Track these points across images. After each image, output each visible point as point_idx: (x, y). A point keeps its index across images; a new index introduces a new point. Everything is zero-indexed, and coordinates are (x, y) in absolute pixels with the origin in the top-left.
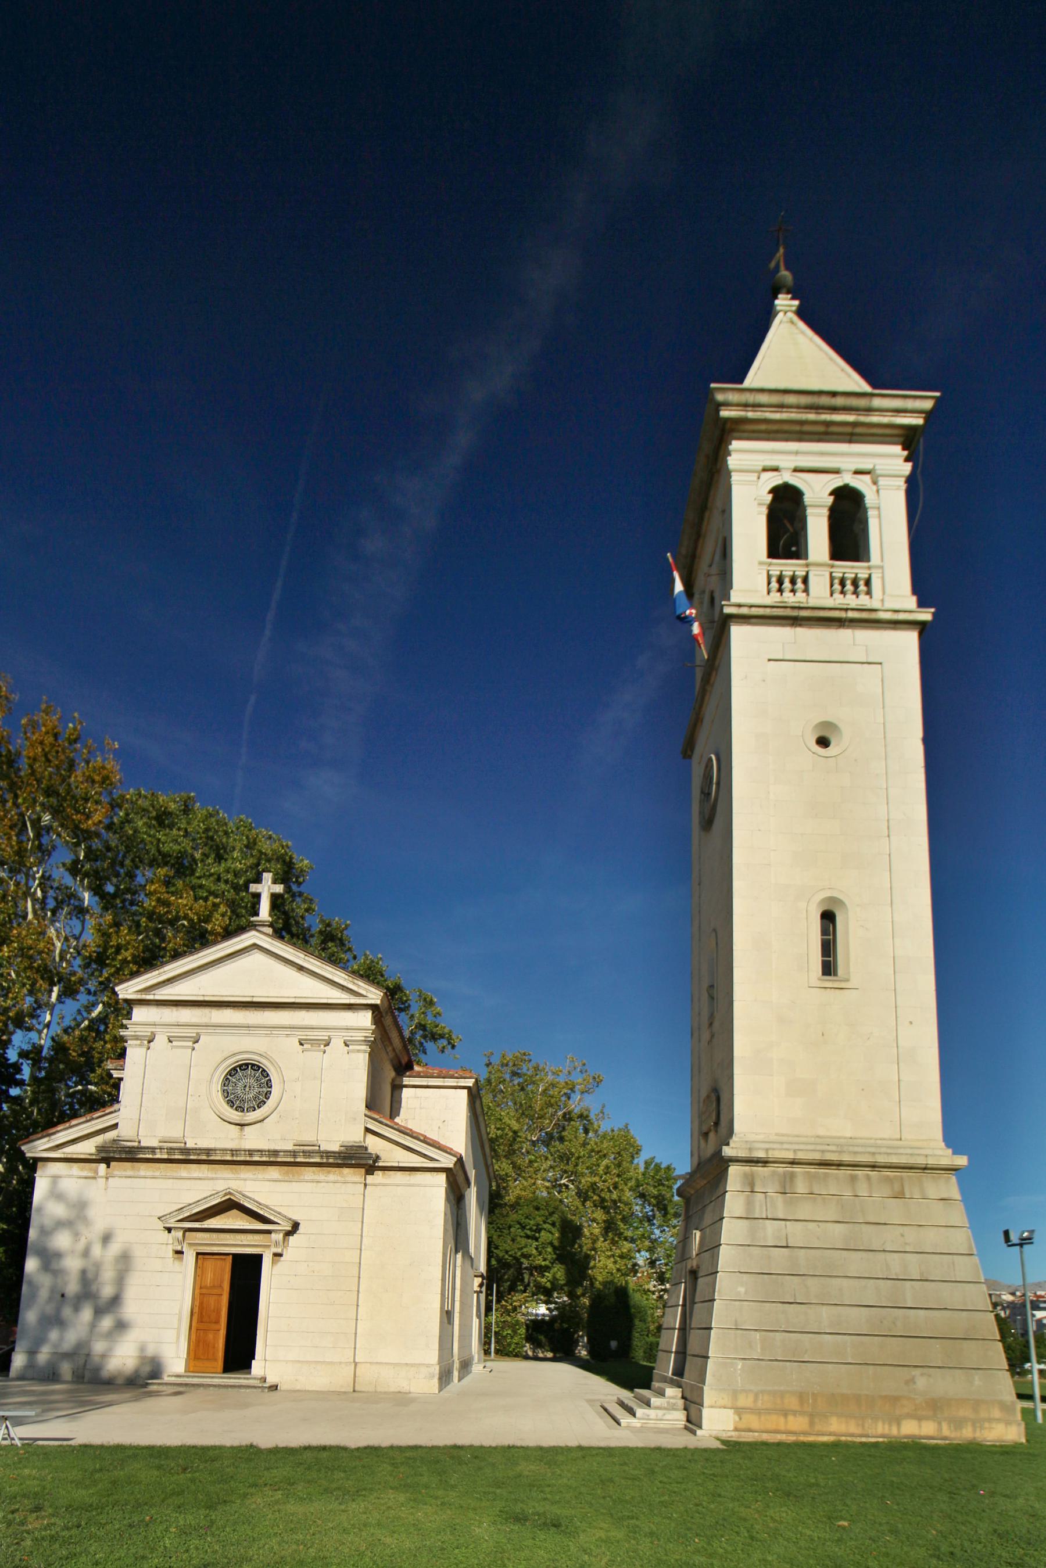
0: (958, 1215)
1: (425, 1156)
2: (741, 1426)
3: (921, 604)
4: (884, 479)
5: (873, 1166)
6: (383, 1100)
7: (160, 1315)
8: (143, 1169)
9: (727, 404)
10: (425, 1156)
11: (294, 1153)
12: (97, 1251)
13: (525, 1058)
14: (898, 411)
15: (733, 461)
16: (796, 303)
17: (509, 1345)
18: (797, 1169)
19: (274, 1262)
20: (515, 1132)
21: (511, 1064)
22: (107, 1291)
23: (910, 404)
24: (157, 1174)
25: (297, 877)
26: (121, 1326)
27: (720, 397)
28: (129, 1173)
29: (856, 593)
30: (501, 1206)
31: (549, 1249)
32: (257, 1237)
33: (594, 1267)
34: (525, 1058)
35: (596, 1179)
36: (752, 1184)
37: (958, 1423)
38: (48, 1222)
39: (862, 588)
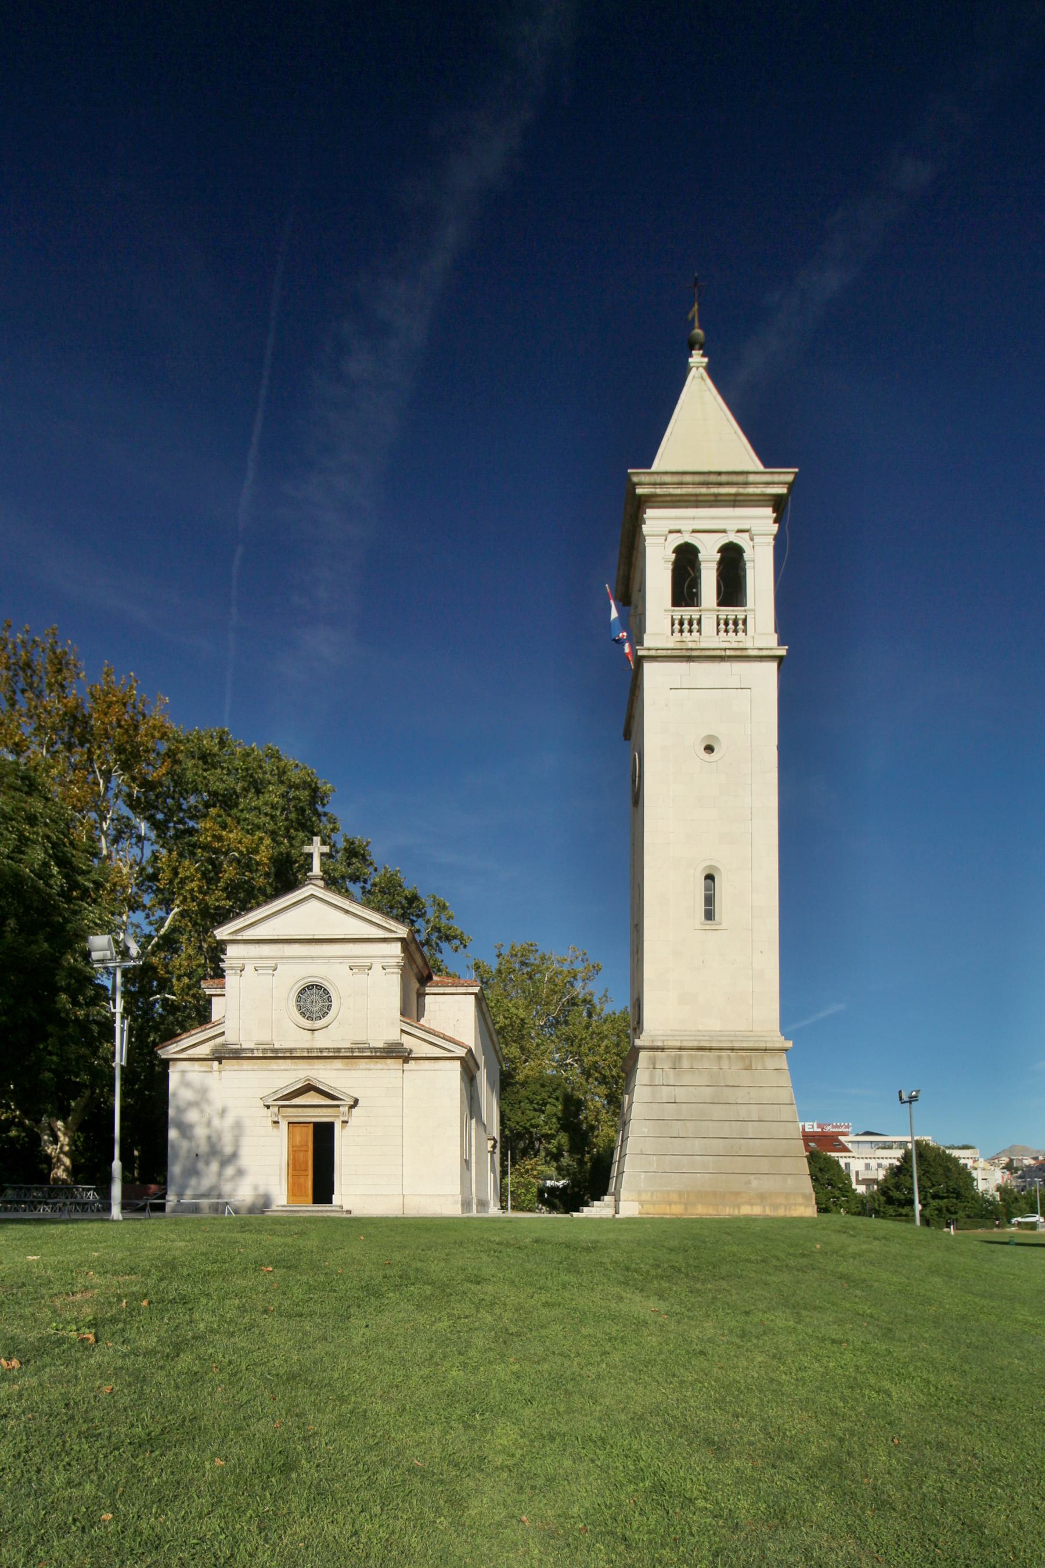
0: (785, 1079)
1: (444, 1049)
2: (643, 1211)
3: (781, 642)
4: (757, 533)
5: (732, 1049)
6: (412, 1007)
7: (263, 1170)
9: (640, 484)
10: (444, 1049)
11: (352, 1050)
12: (216, 1122)
13: (532, 949)
14: (768, 483)
15: (646, 529)
16: (706, 360)
17: (523, 1202)
18: (684, 1053)
19: (342, 1127)
20: (522, 1020)
21: (519, 954)
22: (228, 1150)
23: (776, 478)
24: (256, 1067)
25: (322, 799)
26: (240, 1173)
27: (635, 479)
28: (236, 1067)
29: (736, 631)
30: (513, 1084)
31: (554, 1120)
32: (329, 1110)
33: (597, 1137)
34: (532, 949)
35: (597, 1058)
36: (654, 1064)
37: (775, 1207)
38: (182, 1104)
39: (741, 626)
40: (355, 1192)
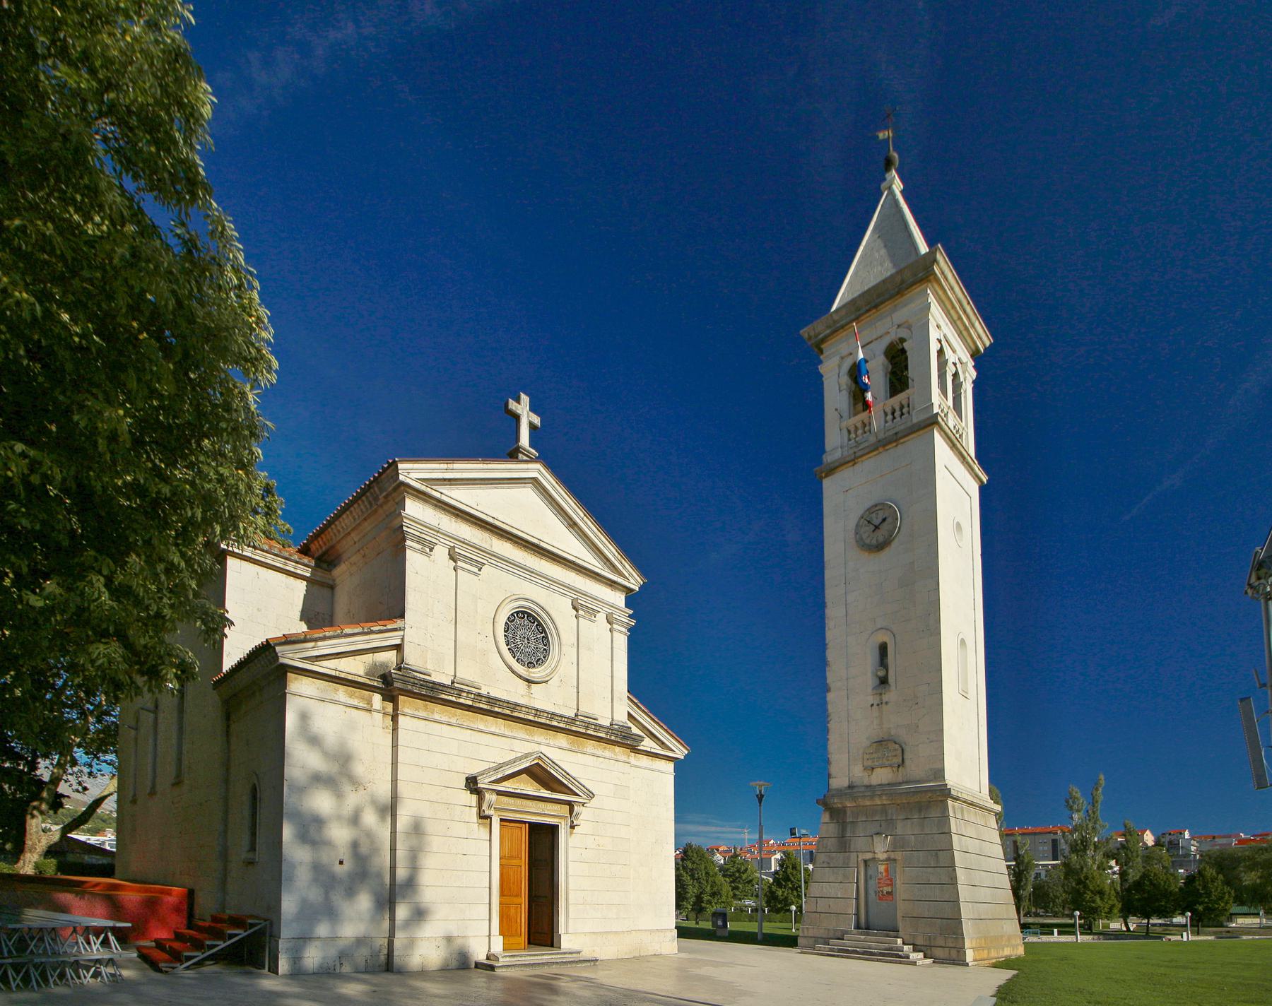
8: (439, 712)
26: (420, 914)
28: (423, 714)
40: (578, 929)
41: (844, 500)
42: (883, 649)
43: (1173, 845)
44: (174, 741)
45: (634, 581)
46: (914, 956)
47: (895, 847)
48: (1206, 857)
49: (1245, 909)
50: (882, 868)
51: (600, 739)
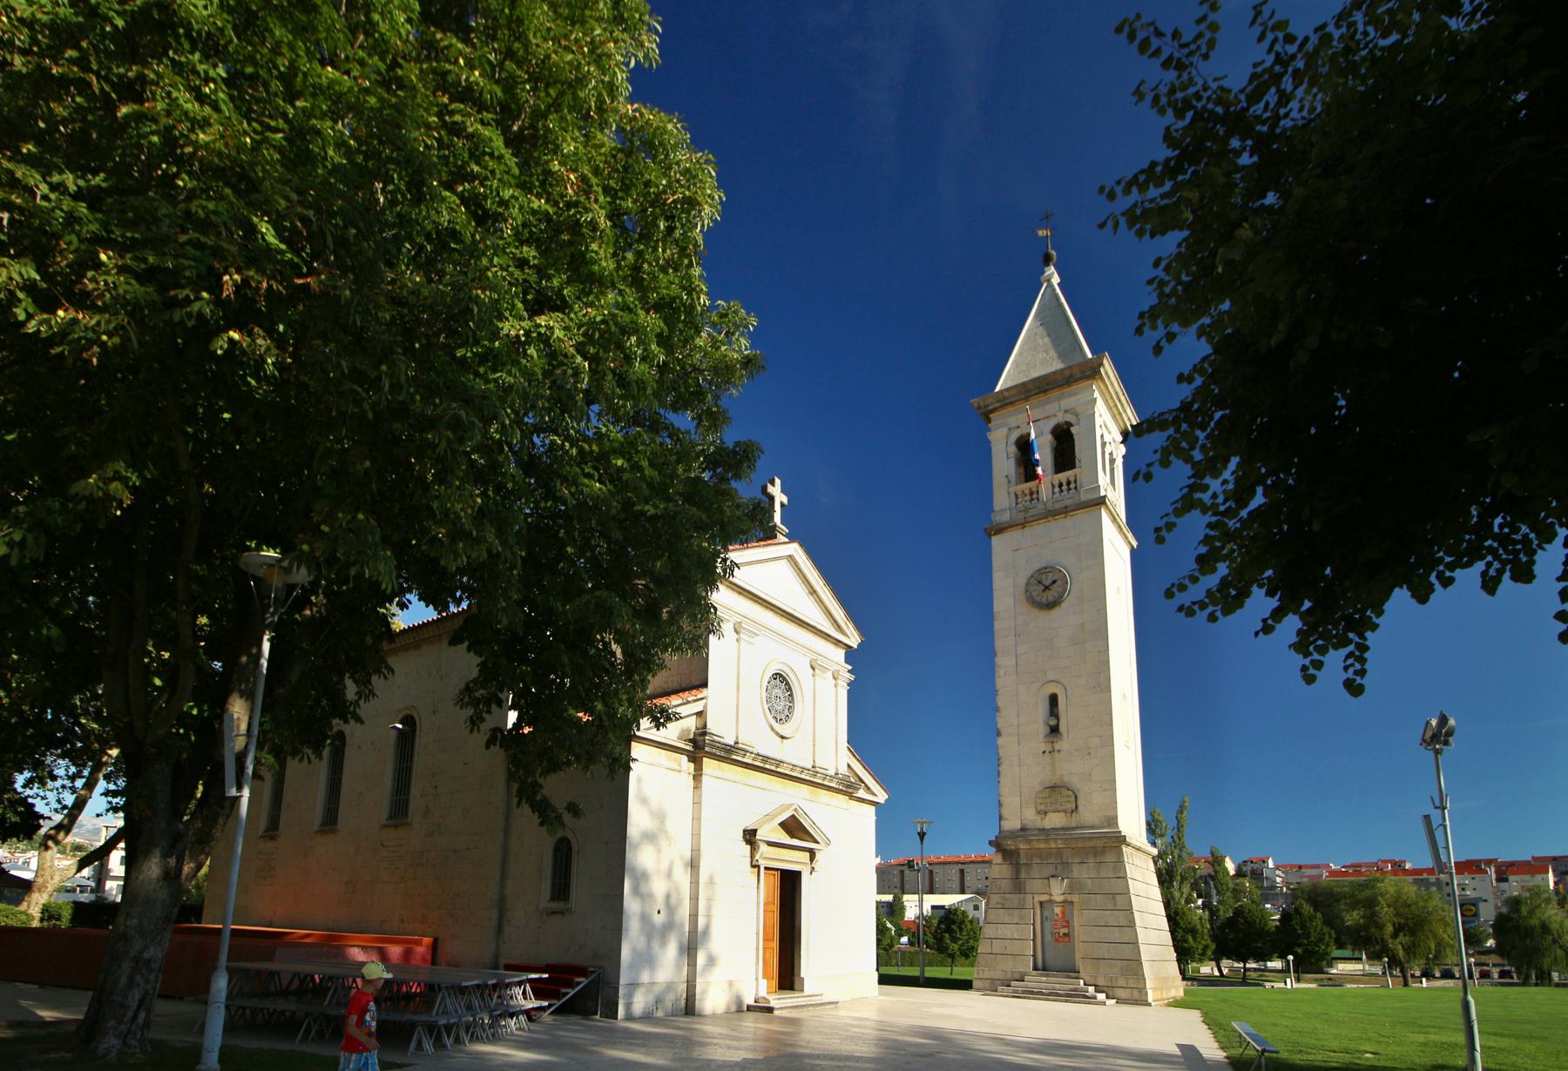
41: (1011, 560)
42: (1053, 700)
43: (1257, 875)
44: (415, 791)
45: (854, 640)
46: (1101, 997)
47: (1072, 889)
48: (1296, 893)
49: (1347, 953)
50: (1058, 910)
51: (829, 788)
